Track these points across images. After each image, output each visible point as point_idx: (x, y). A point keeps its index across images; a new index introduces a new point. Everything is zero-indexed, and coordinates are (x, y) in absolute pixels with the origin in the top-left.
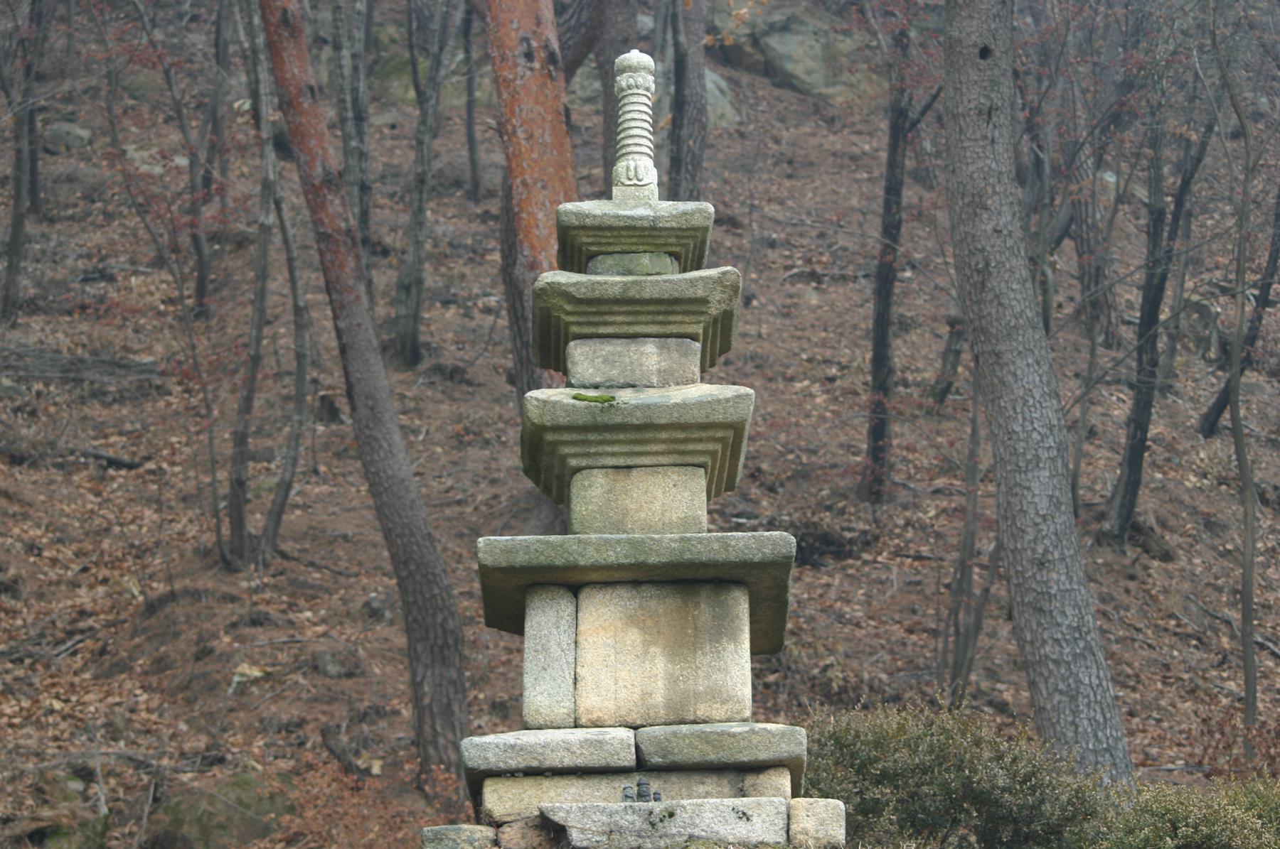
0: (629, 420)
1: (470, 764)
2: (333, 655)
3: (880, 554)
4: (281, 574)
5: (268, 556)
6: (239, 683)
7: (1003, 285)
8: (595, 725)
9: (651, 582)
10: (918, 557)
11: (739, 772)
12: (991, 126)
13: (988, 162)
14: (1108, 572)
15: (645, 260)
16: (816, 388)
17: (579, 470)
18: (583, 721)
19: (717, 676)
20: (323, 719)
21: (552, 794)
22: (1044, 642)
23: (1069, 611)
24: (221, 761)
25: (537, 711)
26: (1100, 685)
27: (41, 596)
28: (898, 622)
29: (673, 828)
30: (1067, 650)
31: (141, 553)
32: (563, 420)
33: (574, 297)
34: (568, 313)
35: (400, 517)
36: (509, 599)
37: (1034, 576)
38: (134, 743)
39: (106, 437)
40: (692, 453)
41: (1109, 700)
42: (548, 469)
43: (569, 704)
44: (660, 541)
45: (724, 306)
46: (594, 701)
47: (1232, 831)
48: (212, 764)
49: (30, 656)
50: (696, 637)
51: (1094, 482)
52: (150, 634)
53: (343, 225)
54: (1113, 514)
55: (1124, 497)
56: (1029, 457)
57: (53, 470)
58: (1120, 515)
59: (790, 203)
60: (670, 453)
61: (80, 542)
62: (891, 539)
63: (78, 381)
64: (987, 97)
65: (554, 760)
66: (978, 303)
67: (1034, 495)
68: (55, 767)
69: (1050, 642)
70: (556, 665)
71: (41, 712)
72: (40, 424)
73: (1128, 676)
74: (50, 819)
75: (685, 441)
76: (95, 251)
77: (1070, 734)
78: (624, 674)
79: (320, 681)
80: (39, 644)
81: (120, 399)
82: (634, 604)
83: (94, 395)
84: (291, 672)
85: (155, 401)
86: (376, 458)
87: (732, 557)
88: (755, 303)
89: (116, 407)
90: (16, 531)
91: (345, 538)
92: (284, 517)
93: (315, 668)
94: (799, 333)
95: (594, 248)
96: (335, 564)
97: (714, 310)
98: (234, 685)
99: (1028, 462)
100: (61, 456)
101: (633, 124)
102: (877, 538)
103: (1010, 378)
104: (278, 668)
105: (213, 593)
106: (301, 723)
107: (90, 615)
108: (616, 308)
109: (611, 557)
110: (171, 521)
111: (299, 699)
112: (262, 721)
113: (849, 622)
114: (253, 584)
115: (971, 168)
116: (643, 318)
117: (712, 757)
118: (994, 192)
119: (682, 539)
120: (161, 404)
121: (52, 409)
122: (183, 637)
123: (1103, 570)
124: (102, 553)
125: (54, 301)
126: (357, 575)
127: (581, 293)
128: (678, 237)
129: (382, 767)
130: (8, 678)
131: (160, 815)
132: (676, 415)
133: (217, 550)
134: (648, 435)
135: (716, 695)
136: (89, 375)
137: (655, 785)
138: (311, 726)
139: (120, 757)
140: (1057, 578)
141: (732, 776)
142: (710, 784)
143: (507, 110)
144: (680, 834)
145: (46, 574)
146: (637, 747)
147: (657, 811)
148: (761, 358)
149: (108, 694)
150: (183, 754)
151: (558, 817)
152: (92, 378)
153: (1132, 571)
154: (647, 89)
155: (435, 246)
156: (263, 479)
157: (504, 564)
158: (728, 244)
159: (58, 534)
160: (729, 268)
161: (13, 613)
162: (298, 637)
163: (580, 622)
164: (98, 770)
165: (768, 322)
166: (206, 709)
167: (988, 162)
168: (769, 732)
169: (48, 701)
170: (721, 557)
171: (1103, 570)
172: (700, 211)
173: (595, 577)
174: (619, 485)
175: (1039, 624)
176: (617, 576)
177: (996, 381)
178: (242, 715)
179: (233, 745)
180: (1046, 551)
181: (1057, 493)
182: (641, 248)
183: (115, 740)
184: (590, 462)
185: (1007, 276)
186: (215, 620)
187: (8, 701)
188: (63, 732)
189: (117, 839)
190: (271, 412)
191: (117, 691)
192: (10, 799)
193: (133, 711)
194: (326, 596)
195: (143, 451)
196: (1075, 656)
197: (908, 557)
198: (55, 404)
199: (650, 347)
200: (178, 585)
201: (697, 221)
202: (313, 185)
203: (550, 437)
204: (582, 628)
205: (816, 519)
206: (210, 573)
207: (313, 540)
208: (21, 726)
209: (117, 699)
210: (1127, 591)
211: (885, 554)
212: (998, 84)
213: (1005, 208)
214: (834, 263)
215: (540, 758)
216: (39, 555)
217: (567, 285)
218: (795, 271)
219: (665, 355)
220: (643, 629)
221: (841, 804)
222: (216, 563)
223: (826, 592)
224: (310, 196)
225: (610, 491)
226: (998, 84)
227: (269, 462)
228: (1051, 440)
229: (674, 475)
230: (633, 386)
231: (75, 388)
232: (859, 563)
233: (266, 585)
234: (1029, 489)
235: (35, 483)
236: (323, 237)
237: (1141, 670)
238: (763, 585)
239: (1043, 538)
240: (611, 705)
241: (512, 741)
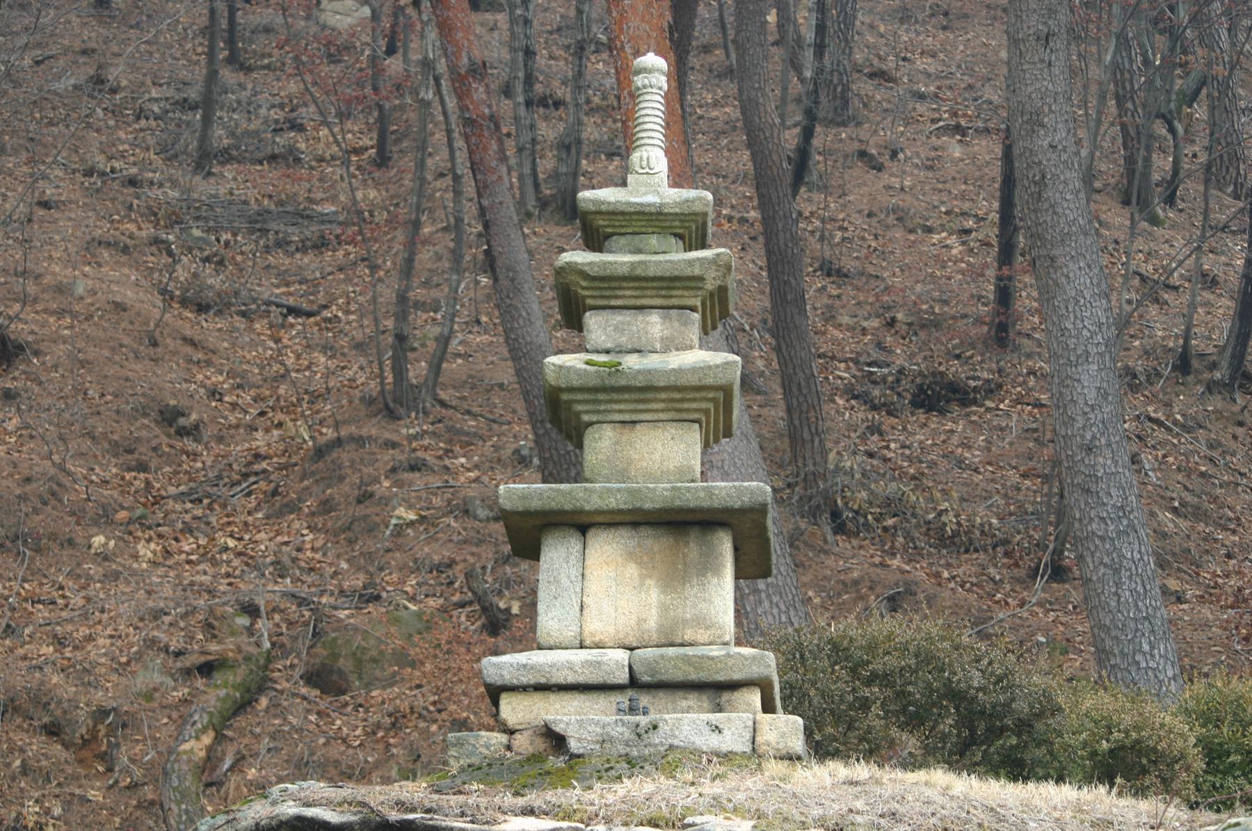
0: (632, 383)
1: (488, 680)
2: (483, 500)
3: (1003, 402)
4: (440, 421)
5: (428, 405)
6: (395, 525)
7: (1057, 195)
9: (647, 524)
10: (1038, 405)
11: (717, 690)
12: (1048, 51)
13: (1045, 83)
14: (1217, 419)
15: (653, 240)
16: (952, 240)
17: (591, 424)
18: (587, 643)
19: (703, 605)
20: (471, 560)
21: (558, 706)
22: (1091, 519)
23: (1114, 492)
24: (377, 598)
25: (548, 634)
26: (1142, 559)
27: (220, 439)
28: (1015, 468)
29: (656, 738)
30: (1112, 528)
31: (315, 397)
32: (576, 383)
33: (588, 275)
34: (584, 288)
35: (538, 380)
36: (528, 535)
37: (1083, 459)
38: (299, 580)
39: (287, 285)
40: (688, 410)
41: (1149, 573)
42: (560, 424)
43: (576, 628)
44: (654, 489)
45: (719, 282)
46: (596, 626)
47: (1159, 736)
48: (368, 601)
49: (208, 496)
51: (1212, 330)
52: (317, 477)
53: (487, 111)
54: (1225, 364)
55: (1234, 348)
56: (1079, 352)
57: (237, 318)
58: (1231, 364)
59: (942, 56)
60: (669, 410)
61: (258, 387)
62: (1014, 387)
63: (264, 231)
64: (1045, 23)
65: (560, 677)
66: (1035, 211)
67: (1083, 387)
68: (224, 604)
69: (1096, 520)
70: (565, 594)
71: (217, 549)
72: (227, 273)
73: (1230, 519)
74: (217, 652)
75: (682, 400)
76: (287, 101)
77: (1113, 604)
79: (470, 523)
80: (217, 485)
81: (303, 249)
82: (632, 543)
83: (279, 244)
84: (444, 515)
85: (334, 251)
86: (516, 325)
87: (716, 504)
88: (901, 156)
89: (298, 256)
90: (200, 377)
91: (501, 386)
92: (444, 365)
93: (466, 512)
94: (940, 186)
95: (610, 230)
96: (491, 412)
97: (710, 285)
98: (391, 527)
99: (1078, 357)
100: (244, 304)
101: (646, 119)
102: (1000, 386)
103: (1063, 279)
104: (432, 511)
105: (376, 440)
106: (451, 564)
107: (265, 458)
108: (625, 284)
109: (612, 503)
110: (343, 368)
111: (451, 541)
112: (416, 561)
113: (969, 467)
114: (411, 431)
115: (1029, 89)
116: (649, 293)
117: (693, 676)
118: (1050, 110)
119: (673, 488)
120: (340, 254)
121: (239, 258)
122: (347, 480)
123: (1213, 416)
124: (278, 398)
125: (246, 151)
126: (509, 423)
127: (594, 272)
128: (681, 221)
129: (521, 607)
130: (188, 518)
131: (319, 650)
132: (673, 378)
133: (380, 399)
134: (650, 395)
135: (701, 622)
136: (273, 226)
137: (644, 700)
138: (459, 567)
139: (284, 594)
140: (1103, 462)
141: (711, 693)
142: (692, 700)
143: (616, 27)
144: (662, 744)
145: (226, 418)
146: (630, 667)
147: (643, 723)
148: (903, 210)
149: (278, 533)
150: (342, 592)
151: (559, 729)
152: (276, 228)
153: (1240, 418)
154: (660, 88)
155: (604, 98)
156: (425, 327)
157: (521, 509)
158: (878, 97)
159: (238, 380)
160: (722, 250)
161: (194, 456)
162: (452, 483)
164: (262, 608)
165: (912, 174)
166: (365, 549)
167: (1045, 83)
169: (222, 539)
170: (706, 504)
171: (1213, 416)
172: (700, 199)
173: (600, 519)
174: (624, 438)
175: (1087, 503)
176: (618, 519)
177: (1051, 282)
178: (398, 555)
179: (387, 583)
180: (1094, 437)
181: (1105, 385)
182: (650, 230)
183: (282, 577)
184: (601, 417)
185: (1061, 187)
186: (377, 465)
187: (187, 539)
188: (235, 569)
189: (280, 671)
190: (439, 264)
191: (286, 530)
192: (183, 634)
193: (299, 550)
194: (481, 443)
195: (321, 298)
196: (1119, 532)
197: (1028, 404)
198: (242, 253)
199: (655, 318)
200: (344, 432)
201: (698, 208)
202: (459, 74)
203: (565, 397)
204: (588, 563)
205: (942, 368)
206: (374, 421)
207: (472, 389)
208: (198, 562)
209: (286, 539)
210: (1235, 437)
211: (1007, 401)
212: (1055, 12)
213: (1060, 126)
214: (978, 116)
216: (220, 400)
217: (583, 264)
218: (941, 124)
220: (640, 564)
221: (800, 720)
222: (380, 411)
223: (949, 439)
224: (457, 85)
225: (617, 443)
226: (1055, 12)
227: (435, 312)
228: (1099, 336)
229: (672, 429)
230: (639, 351)
231: (260, 237)
232: (983, 410)
233: (425, 432)
234: (1079, 381)
235: (220, 330)
236: (469, 122)
237: (1242, 513)
238: (746, 531)
239: (1091, 425)
240: (611, 629)
241: (524, 662)
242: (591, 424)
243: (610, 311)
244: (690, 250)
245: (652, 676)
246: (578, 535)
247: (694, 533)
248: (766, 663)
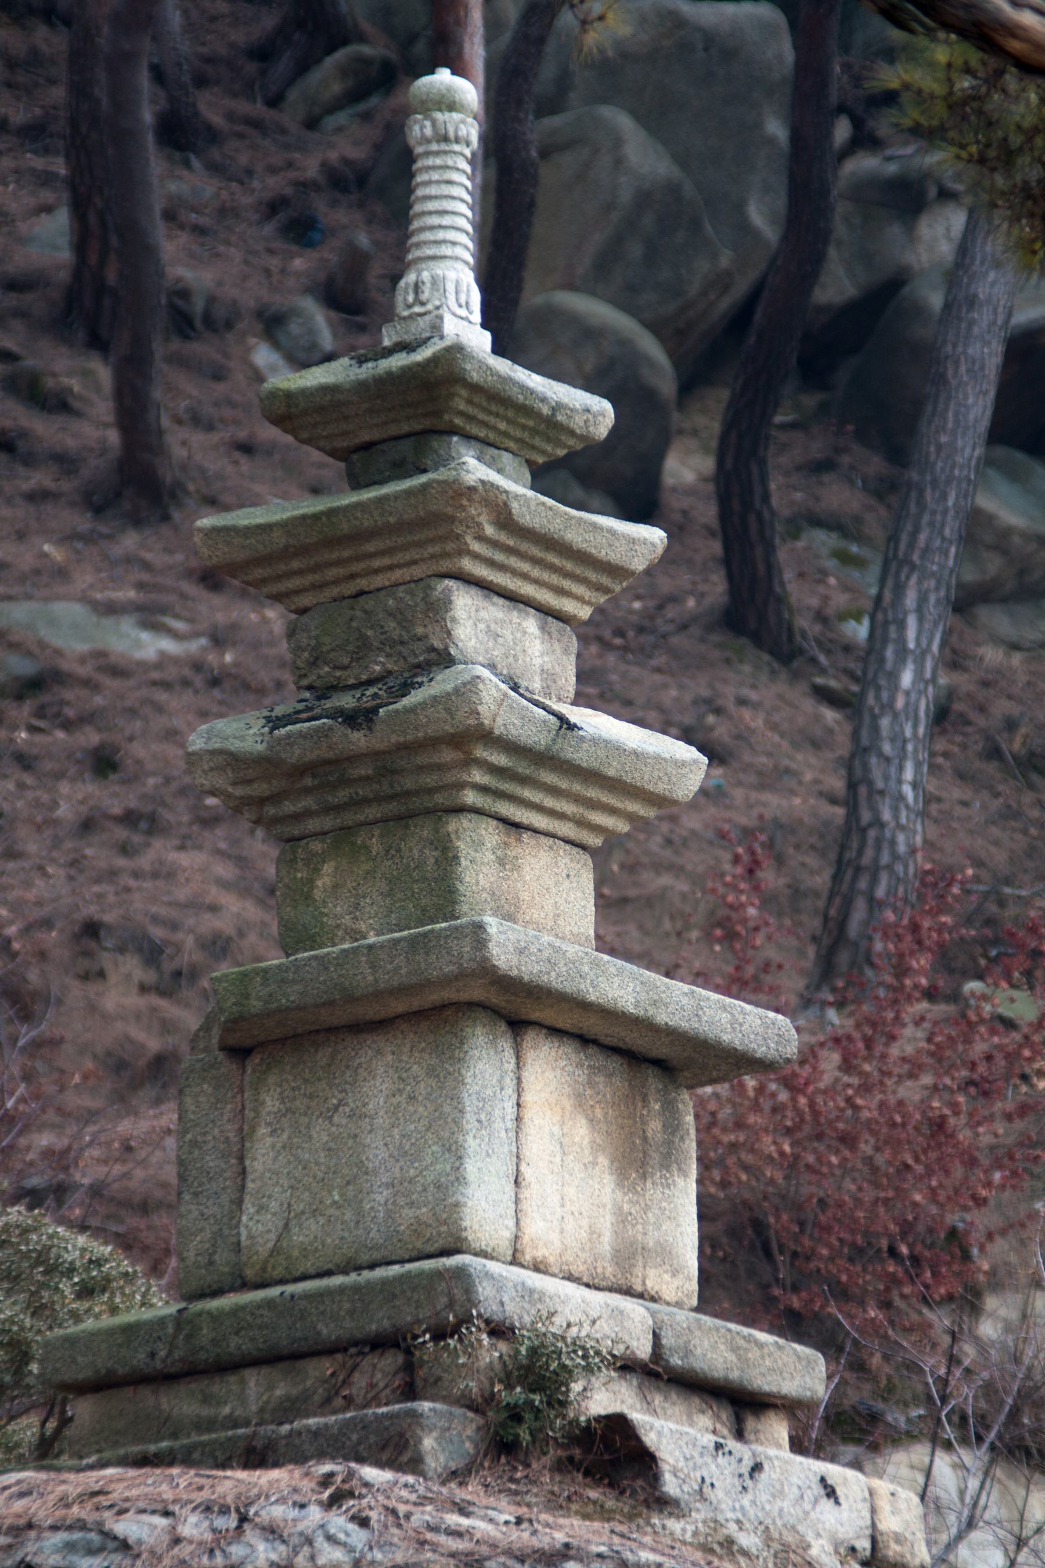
95: (458, 421)
146: (656, 1336)
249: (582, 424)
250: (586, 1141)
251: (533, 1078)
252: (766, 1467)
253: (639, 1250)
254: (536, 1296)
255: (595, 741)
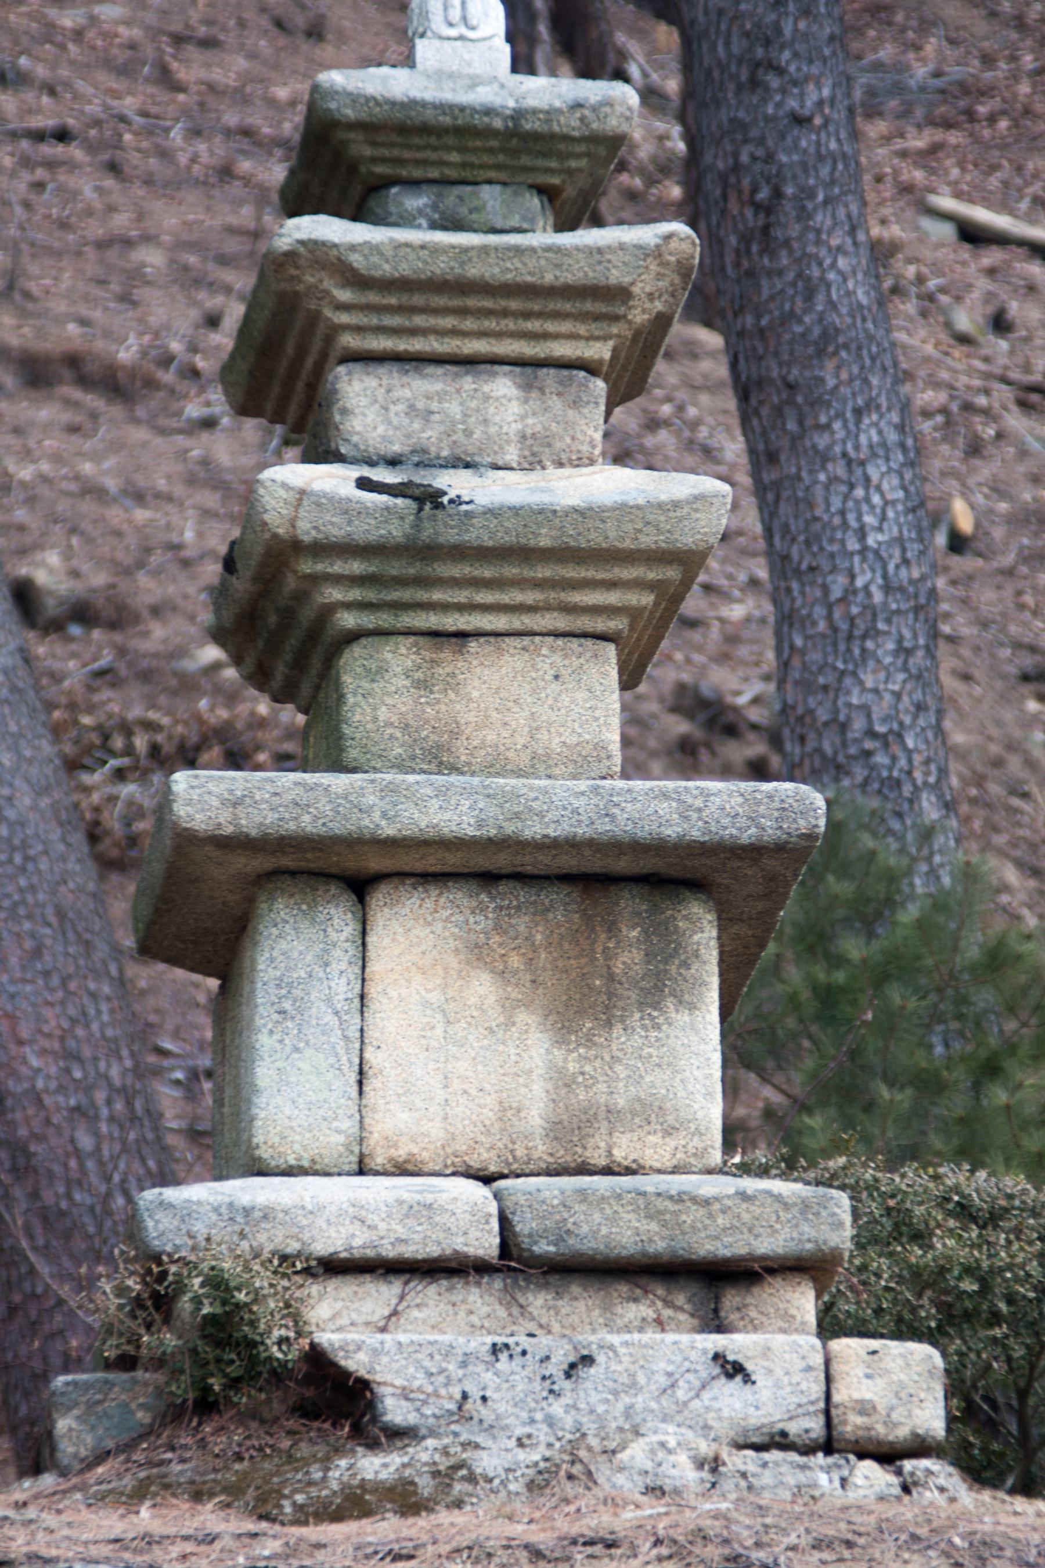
8: (403, 1169)
11: (712, 1283)
15: (490, 196)
17: (354, 636)
18: (379, 1160)
33: (354, 272)
42: (285, 630)
43: (349, 1125)
46: (400, 1121)
50: (611, 995)
78: (462, 1066)
82: (483, 923)
95: (379, 169)
135: (651, 1114)
146: (504, 1220)
163: (371, 953)
168: (778, 1198)
199: (503, 386)
201: (613, 124)
204: (375, 967)
215: (306, 1236)
219: (534, 404)
229: (550, 658)
230: (467, 466)
240: (436, 1131)
242: (354, 636)
243: (395, 367)
244: (572, 228)
245: (559, 1241)
246: (348, 899)
247: (629, 903)
248: (819, 1214)
249: (578, 123)
250: (491, 999)
251: (386, 941)
252: (601, 1359)
253: (602, 1115)
254: (257, 1214)
255: (491, 512)
